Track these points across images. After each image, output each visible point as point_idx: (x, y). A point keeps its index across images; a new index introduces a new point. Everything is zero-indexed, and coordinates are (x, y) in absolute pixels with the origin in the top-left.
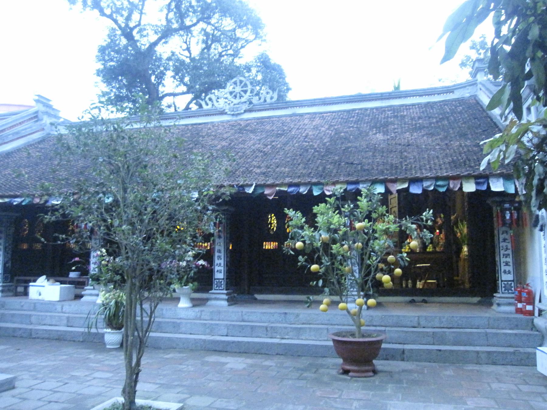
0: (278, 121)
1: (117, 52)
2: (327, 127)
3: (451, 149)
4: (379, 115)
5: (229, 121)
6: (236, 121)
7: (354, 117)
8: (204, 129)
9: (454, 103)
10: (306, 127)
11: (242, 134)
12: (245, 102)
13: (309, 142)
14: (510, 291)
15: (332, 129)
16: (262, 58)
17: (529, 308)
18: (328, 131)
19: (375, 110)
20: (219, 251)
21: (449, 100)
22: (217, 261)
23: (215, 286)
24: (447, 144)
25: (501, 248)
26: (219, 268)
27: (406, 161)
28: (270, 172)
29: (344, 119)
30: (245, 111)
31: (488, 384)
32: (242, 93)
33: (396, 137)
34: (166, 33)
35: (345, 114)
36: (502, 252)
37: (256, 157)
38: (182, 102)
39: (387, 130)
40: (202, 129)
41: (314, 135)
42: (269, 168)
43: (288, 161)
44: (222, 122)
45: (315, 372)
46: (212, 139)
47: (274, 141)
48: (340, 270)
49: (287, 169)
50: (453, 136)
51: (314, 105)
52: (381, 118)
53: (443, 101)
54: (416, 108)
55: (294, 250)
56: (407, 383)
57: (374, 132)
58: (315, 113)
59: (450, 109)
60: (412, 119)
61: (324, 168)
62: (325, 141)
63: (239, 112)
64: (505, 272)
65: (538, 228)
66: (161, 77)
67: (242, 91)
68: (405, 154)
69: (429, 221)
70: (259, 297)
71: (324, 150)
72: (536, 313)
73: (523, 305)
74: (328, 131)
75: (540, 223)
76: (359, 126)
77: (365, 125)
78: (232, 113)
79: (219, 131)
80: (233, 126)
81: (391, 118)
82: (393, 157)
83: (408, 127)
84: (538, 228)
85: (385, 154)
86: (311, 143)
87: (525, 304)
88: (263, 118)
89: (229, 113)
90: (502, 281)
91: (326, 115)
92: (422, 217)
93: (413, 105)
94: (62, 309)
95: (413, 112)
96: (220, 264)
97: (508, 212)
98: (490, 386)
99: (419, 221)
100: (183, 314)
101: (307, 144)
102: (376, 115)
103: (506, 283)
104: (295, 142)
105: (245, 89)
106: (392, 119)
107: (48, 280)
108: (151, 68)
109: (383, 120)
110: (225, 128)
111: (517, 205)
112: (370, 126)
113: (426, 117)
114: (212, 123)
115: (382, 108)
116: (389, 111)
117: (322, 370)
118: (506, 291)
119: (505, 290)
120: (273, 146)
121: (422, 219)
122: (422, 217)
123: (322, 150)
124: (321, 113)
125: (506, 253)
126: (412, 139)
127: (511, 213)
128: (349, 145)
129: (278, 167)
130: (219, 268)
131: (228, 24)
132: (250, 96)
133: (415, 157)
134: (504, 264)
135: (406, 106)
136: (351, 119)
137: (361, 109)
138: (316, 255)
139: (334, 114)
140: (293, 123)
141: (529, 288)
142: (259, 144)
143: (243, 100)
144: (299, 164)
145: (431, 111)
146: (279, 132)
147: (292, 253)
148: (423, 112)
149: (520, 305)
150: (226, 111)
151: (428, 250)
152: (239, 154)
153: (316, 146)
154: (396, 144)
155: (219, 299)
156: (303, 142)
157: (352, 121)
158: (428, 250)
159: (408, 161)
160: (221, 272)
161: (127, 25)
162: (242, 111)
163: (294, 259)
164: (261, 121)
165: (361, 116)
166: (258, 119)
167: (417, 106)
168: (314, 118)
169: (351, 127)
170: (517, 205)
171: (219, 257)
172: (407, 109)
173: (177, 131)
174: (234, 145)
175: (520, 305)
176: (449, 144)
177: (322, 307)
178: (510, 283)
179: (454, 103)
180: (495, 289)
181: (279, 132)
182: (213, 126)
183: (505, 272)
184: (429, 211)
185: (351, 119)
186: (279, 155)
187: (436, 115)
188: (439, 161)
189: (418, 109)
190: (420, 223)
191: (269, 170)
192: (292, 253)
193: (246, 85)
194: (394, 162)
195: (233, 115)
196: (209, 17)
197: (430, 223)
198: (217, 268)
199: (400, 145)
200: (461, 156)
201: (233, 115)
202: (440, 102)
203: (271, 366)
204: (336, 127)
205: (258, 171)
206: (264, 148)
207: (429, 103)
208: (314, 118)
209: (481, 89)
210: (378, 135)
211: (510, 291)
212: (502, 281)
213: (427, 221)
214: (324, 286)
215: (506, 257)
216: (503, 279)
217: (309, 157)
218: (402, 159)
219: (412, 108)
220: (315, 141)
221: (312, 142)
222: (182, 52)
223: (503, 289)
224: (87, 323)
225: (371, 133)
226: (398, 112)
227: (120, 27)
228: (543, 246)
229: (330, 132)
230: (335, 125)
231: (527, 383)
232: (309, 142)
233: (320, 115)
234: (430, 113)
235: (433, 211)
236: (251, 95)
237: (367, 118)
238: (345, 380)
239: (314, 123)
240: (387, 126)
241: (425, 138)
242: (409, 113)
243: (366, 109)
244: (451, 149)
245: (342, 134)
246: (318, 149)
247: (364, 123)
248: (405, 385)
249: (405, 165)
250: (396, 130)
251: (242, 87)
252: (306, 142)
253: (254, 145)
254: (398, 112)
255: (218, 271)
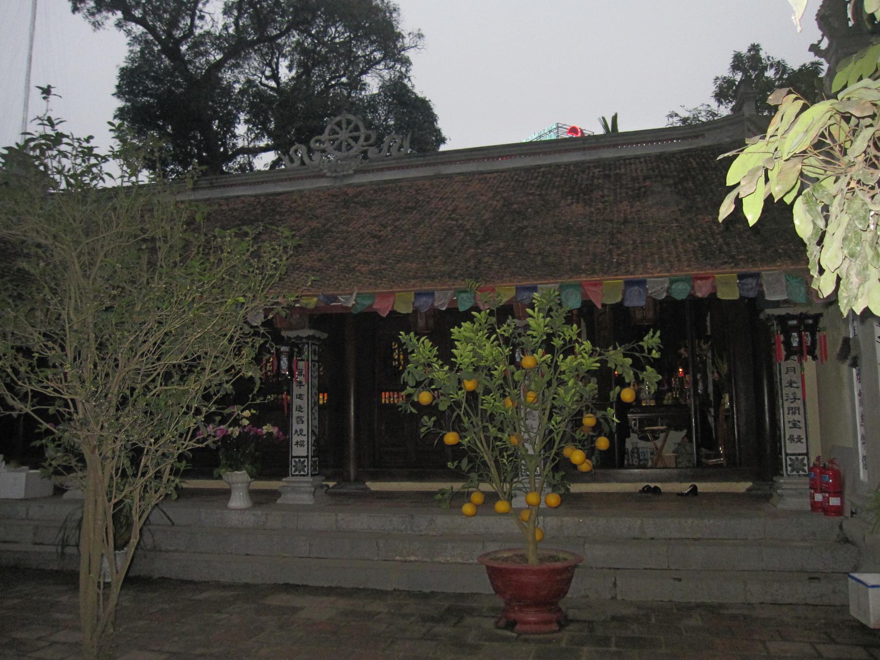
0: (410, 187)
1: (156, 80)
2: (490, 195)
3: (697, 227)
4: (578, 174)
5: (328, 188)
6: (340, 188)
7: (536, 178)
8: (285, 203)
9: (704, 153)
10: (455, 196)
11: (348, 208)
12: (356, 157)
13: (457, 220)
14: (801, 473)
15: (498, 198)
16: (395, 89)
17: (834, 501)
18: (491, 202)
19: (572, 168)
20: (300, 409)
21: (696, 150)
22: (296, 426)
23: (293, 469)
24: (690, 219)
25: (785, 398)
26: (300, 438)
27: (619, 248)
28: (384, 270)
29: (520, 181)
30: (356, 172)
31: (763, 643)
32: (350, 141)
33: (605, 209)
34: (235, 48)
35: (523, 174)
36: (787, 405)
37: (365, 246)
38: (263, 161)
39: (591, 200)
40: (282, 202)
41: (467, 208)
42: (383, 263)
43: (419, 252)
44: (318, 190)
45: (455, 625)
46: (297, 218)
47: (398, 220)
48: (501, 440)
49: (414, 265)
50: (700, 206)
51: (470, 160)
52: (582, 180)
53: (686, 151)
54: (641, 163)
55: (416, 405)
56: (617, 646)
57: (569, 201)
58: (473, 173)
59: (697, 163)
60: (634, 179)
61: (479, 262)
62: (485, 217)
63: (345, 173)
64: (792, 438)
65: (848, 362)
66: (229, 122)
67: (351, 138)
68: (619, 236)
69: (654, 352)
70: (374, 486)
71: (482, 233)
72: (847, 513)
73: (824, 497)
74: (491, 202)
75: (853, 353)
76: (543, 192)
77: (555, 191)
78: (334, 174)
79: (310, 204)
80: (334, 196)
81: (598, 178)
82: (597, 242)
83: (627, 193)
84: (848, 362)
85: (584, 237)
86: (460, 222)
87: (827, 495)
88: (386, 182)
89: (329, 174)
90: (787, 455)
91: (489, 176)
92: (641, 343)
93: (637, 158)
94: (27, 513)
95: (636, 169)
96: (301, 430)
97: (795, 334)
98: (766, 648)
99: (637, 351)
100: (234, 520)
101: (454, 223)
102: (573, 174)
103: (793, 457)
104: (434, 220)
105: (355, 134)
106: (600, 181)
107: (7, 463)
108: (211, 108)
109: (585, 182)
110: (321, 200)
111: (810, 321)
112: (563, 191)
113: (657, 176)
114: (300, 191)
115: (583, 162)
116: (596, 167)
117: (469, 620)
118: (795, 473)
119: (792, 471)
120: (396, 227)
121: (642, 347)
122: (641, 343)
123: (477, 232)
124: (482, 173)
125: (792, 405)
126: (631, 212)
127: (800, 337)
128: (525, 223)
129: (399, 261)
130: (300, 438)
131: (338, 33)
132: (363, 146)
133: (635, 242)
134: (791, 425)
135: (625, 160)
136: (532, 182)
137: (550, 166)
138: (455, 414)
139: (504, 174)
140: (434, 190)
141: (835, 467)
142: (373, 224)
143: (352, 152)
144: (436, 257)
145: (666, 167)
146: (410, 204)
147: (414, 411)
148: (653, 170)
149: (819, 497)
150: (325, 171)
151: (665, 402)
152: (338, 241)
153: (468, 227)
154: (604, 220)
155: (299, 489)
156: (447, 220)
157: (533, 185)
158: (665, 402)
159: (623, 249)
160: (302, 445)
161: (170, 35)
162: (351, 172)
163: (415, 419)
164: (381, 187)
165: (549, 176)
166: (378, 183)
167: (642, 160)
168: (470, 181)
169: (530, 194)
170: (810, 321)
171: (300, 420)
172: (626, 165)
173: (241, 205)
174: (331, 227)
175: (819, 497)
176: (695, 220)
177: (468, 509)
178: (800, 457)
179: (704, 153)
180: (777, 469)
181: (410, 204)
182: (302, 197)
183: (792, 438)
184: (654, 333)
185: (532, 182)
186: (406, 241)
187: (675, 173)
188: (676, 247)
189: (644, 164)
190: (637, 354)
191: (383, 266)
192: (414, 411)
193: (357, 129)
194: (598, 251)
195: (335, 178)
196: (310, 23)
197: (655, 354)
198: (295, 438)
199: (611, 221)
200: (714, 239)
201: (335, 178)
202: (681, 152)
203: (379, 613)
204: (505, 195)
205: (365, 269)
206: (380, 231)
207: (662, 154)
208: (470, 181)
209: (749, 130)
210: (574, 207)
211: (801, 473)
212: (787, 455)
213: (650, 351)
214: (472, 469)
215: (794, 413)
216: (788, 451)
217: (455, 244)
218: (613, 244)
219: (635, 163)
220: (467, 218)
221: (463, 219)
222: (264, 80)
223: (789, 469)
224: (60, 536)
225: (563, 203)
226: (610, 169)
227: (157, 37)
228: (856, 393)
229: (495, 203)
230: (504, 192)
231: (833, 641)
232: (457, 220)
233: (480, 177)
234: (665, 169)
235: (200, 132)
236: (365, 144)
237: (558, 179)
238: (507, 639)
239: (470, 190)
240: (592, 191)
241: (654, 210)
242: (628, 171)
243: (558, 166)
244: (697, 227)
245: (515, 206)
246: (471, 231)
247: (553, 187)
248: (613, 649)
249: (618, 255)
250: (606, 199)
251: (351, 132)
252: (452, 219)
253: (364, 226)
254: (610, 169)
255: (297, 443)
